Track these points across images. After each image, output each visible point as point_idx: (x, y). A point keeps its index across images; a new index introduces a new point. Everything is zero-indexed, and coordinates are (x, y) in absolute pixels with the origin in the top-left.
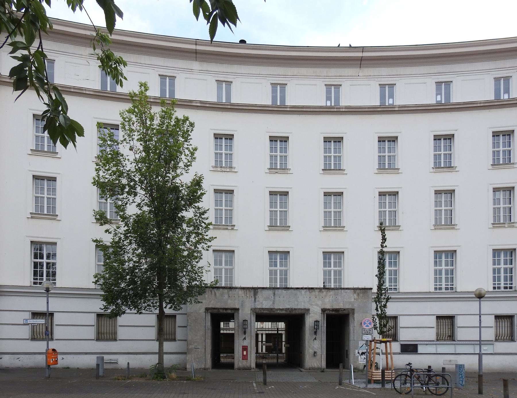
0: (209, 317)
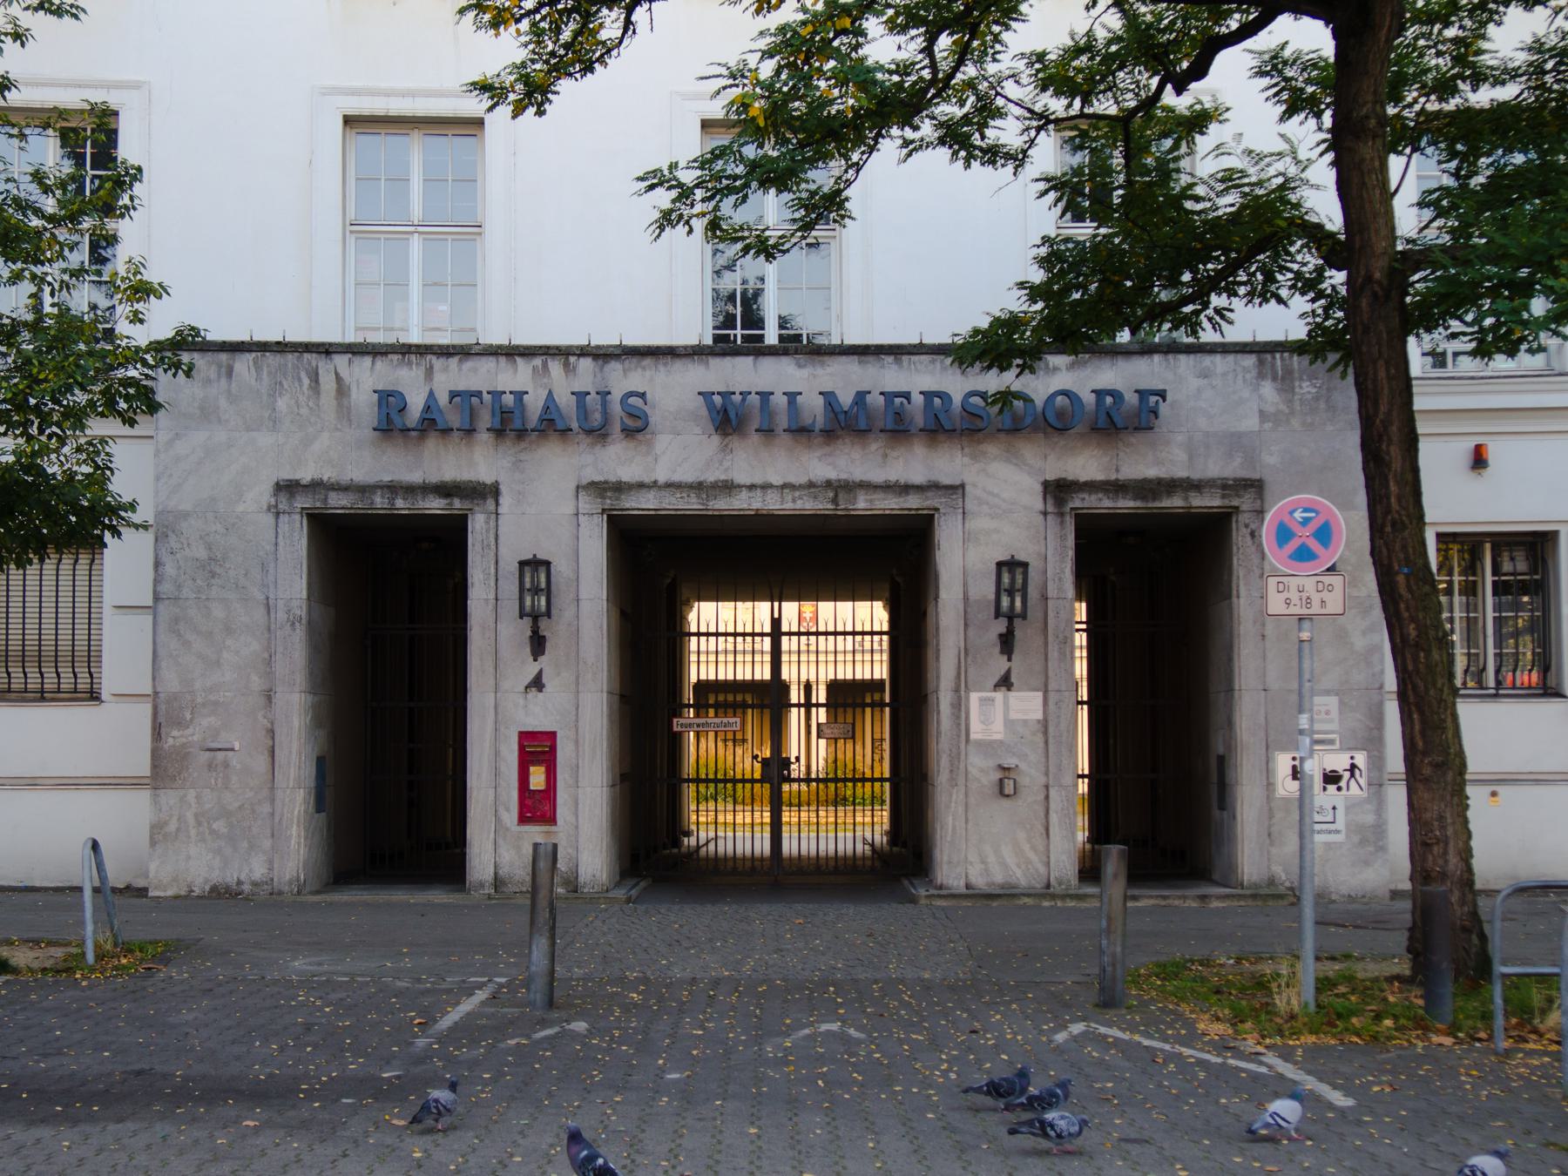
0: (296, 542)
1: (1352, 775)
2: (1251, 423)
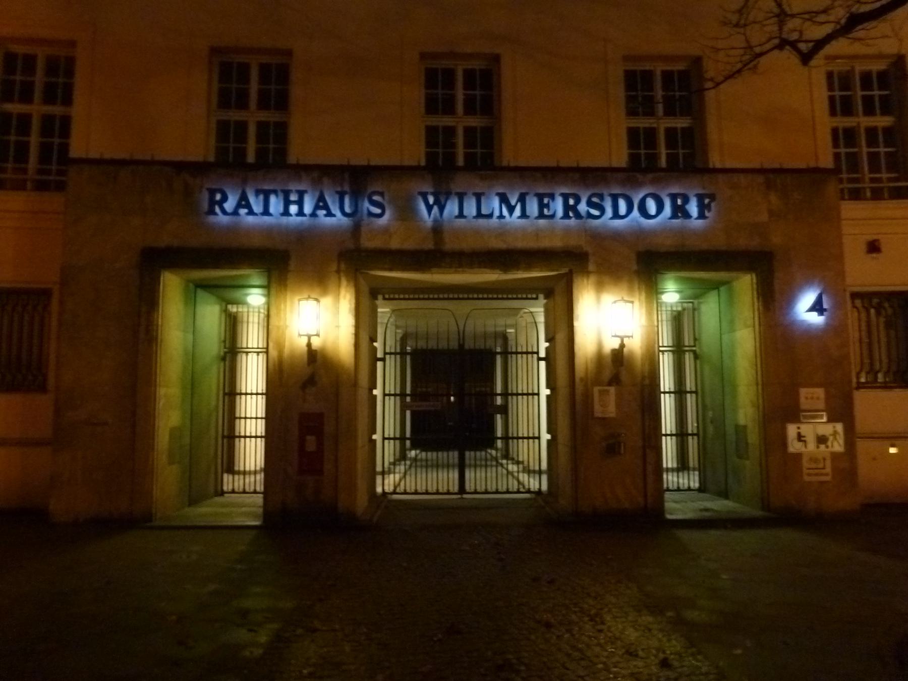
1: (835, 439)
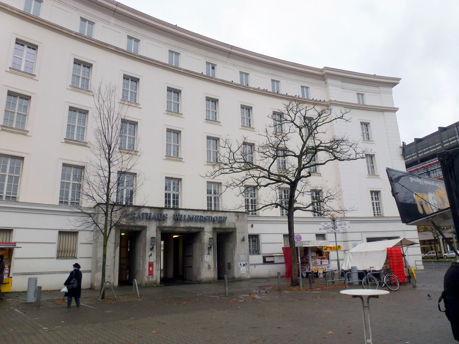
2: (235, 221)
